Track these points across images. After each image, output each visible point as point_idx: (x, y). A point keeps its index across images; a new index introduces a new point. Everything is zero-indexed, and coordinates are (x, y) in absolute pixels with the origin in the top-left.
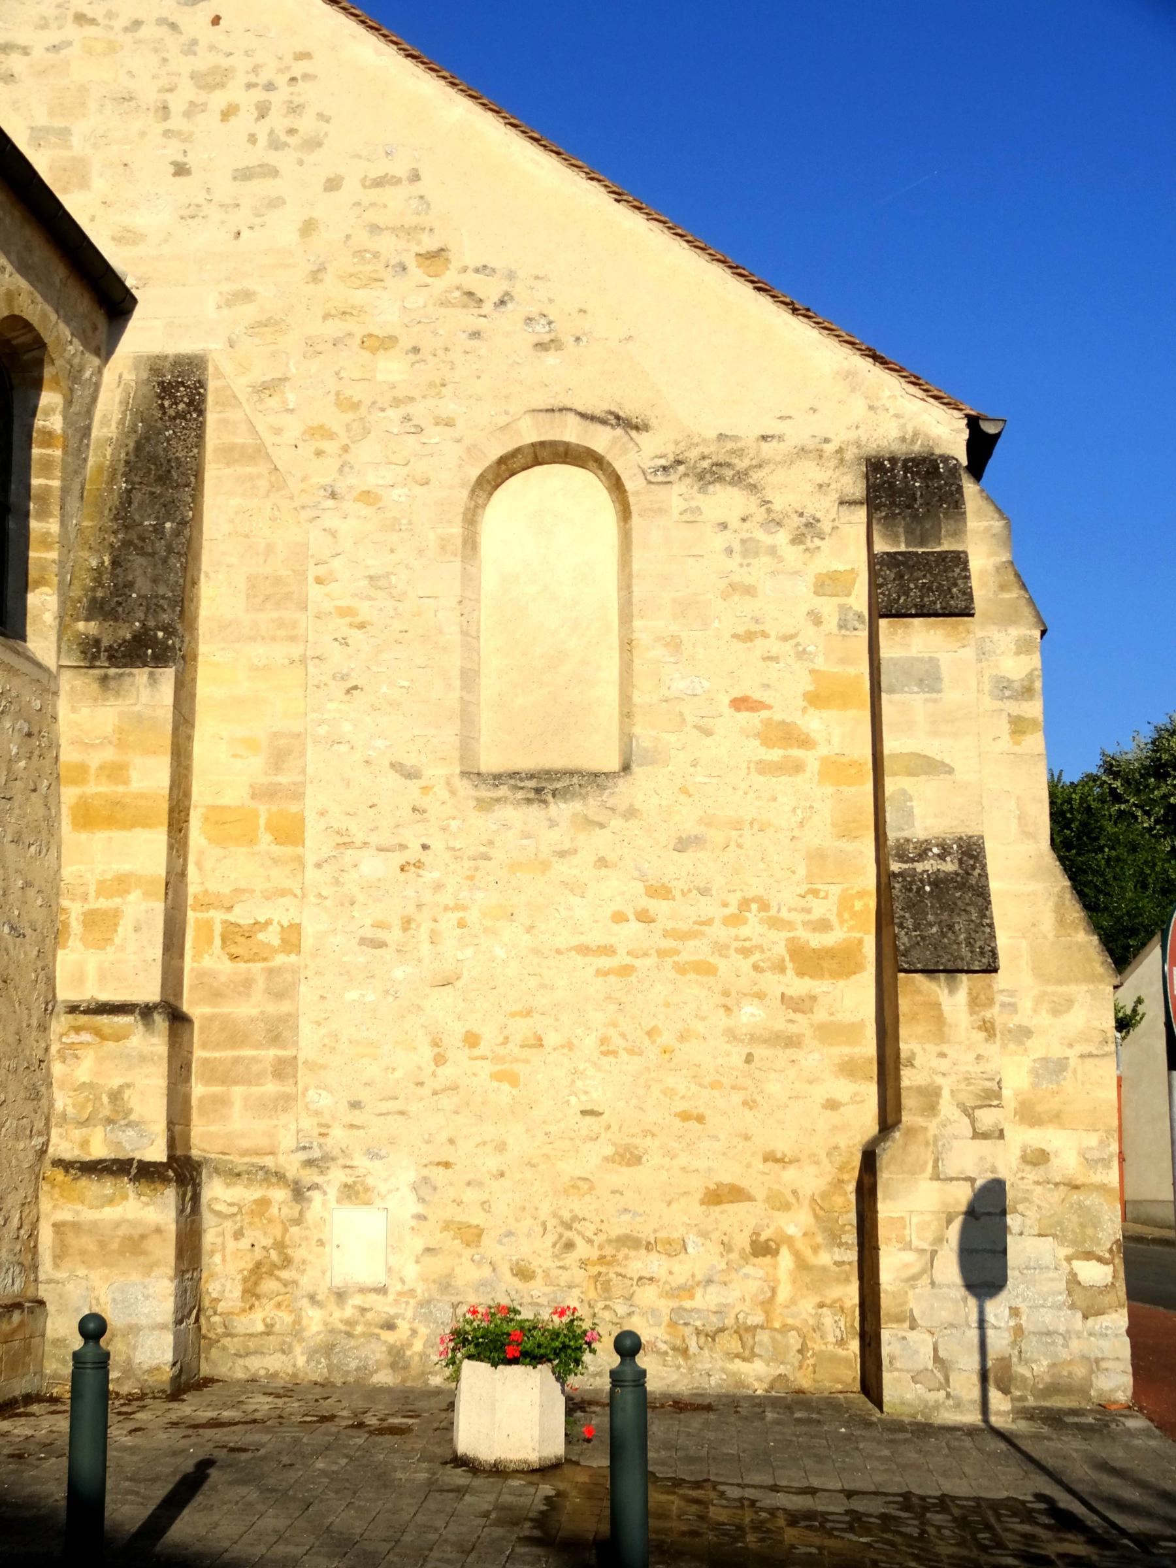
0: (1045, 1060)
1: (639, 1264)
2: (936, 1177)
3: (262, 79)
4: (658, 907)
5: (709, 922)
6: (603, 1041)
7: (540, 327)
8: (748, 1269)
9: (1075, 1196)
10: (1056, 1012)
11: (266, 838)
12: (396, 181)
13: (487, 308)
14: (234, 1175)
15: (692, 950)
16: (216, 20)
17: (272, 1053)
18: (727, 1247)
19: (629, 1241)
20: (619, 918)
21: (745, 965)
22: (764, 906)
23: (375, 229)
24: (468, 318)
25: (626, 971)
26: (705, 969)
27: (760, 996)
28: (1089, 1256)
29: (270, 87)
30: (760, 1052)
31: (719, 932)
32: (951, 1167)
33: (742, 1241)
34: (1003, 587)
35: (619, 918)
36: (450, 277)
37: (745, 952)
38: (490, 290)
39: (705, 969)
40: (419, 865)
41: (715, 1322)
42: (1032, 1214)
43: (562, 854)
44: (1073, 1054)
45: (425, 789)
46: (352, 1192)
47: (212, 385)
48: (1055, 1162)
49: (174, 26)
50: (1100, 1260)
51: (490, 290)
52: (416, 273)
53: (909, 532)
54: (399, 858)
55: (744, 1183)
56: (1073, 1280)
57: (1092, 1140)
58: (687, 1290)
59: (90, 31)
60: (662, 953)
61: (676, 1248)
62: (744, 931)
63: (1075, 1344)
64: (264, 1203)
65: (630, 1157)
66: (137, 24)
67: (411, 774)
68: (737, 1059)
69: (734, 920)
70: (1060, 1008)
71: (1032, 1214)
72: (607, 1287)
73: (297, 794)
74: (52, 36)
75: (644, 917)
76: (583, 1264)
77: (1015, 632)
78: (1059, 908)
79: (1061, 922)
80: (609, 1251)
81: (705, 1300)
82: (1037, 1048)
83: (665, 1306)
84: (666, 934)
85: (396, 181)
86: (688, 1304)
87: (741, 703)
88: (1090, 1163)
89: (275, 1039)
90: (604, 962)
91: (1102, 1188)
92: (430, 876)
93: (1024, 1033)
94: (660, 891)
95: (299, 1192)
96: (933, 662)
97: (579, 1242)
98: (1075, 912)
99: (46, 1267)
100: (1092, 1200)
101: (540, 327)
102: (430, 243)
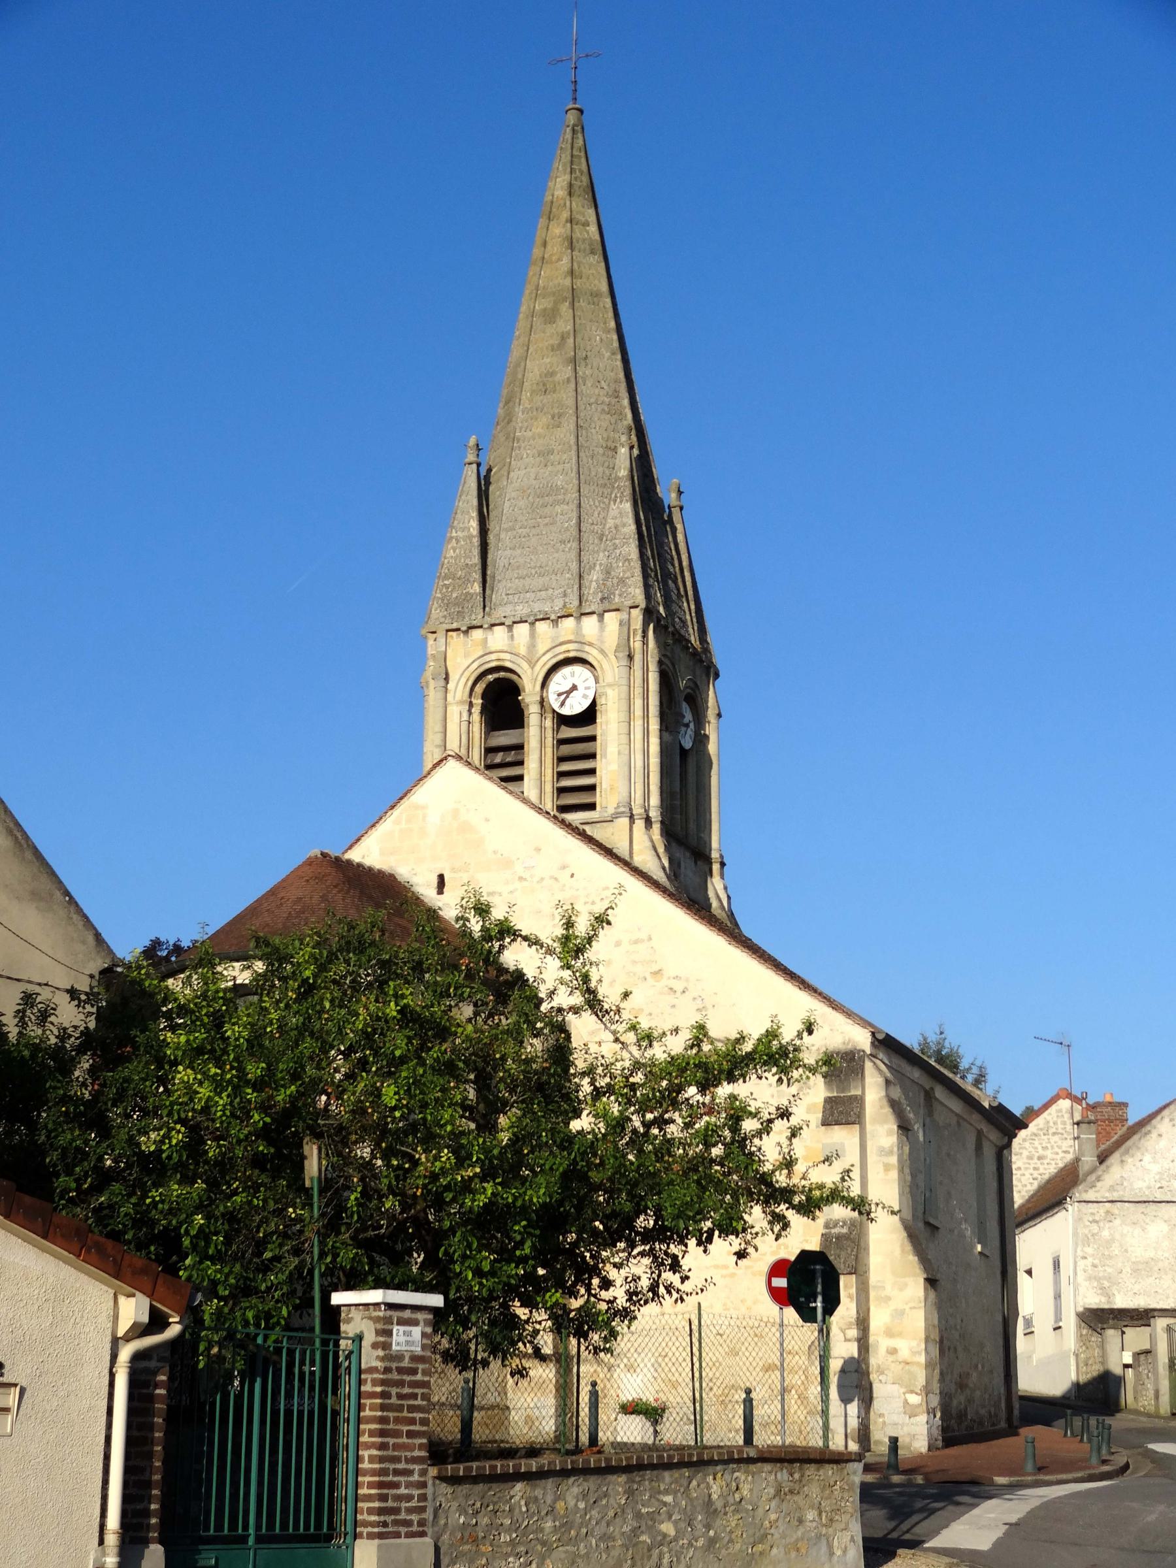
0: (896, 1310)
3: (590, 900)
7: (699, 1001)
9: (907, 1367)
10: (901, 1290)
12: (643, 941)
13: (678, 994)
16: (572, 876)
23: (634, 962)
24: (671, 999)
28: (912, 1392)
29: (593, 903)
34: (881, 1107)
36: (664, 982)
38: (679, 986)
42: (890, 1375)
44: (907, 1307)
46: (630, 1368)
48: (900, 1353)
49: (556, 879)
51: (679, 986)
52: (650, 980)
53: (838, 1087)
57: (914, 1343)
59: (525, 884)
63: (905, 1429)
65: (734, 1353)
66: (542, 879)
70: (902, 1288)
71: (890, 1375)
74: (511, 888)
77: (886, 1127)
78: (902, 1245)
79: (903, 1251)
82: (893, 1305)
85: (643, 941)
88: (914, 1353)
90: (724, 1272)
91: (918, 1364)
93: (888, 1298)
96: (842, 1144)
98: (909, 1247)
99: (510, 1394)
100: (914, 1369)
101: (699, 1001)
102: (655, 968)
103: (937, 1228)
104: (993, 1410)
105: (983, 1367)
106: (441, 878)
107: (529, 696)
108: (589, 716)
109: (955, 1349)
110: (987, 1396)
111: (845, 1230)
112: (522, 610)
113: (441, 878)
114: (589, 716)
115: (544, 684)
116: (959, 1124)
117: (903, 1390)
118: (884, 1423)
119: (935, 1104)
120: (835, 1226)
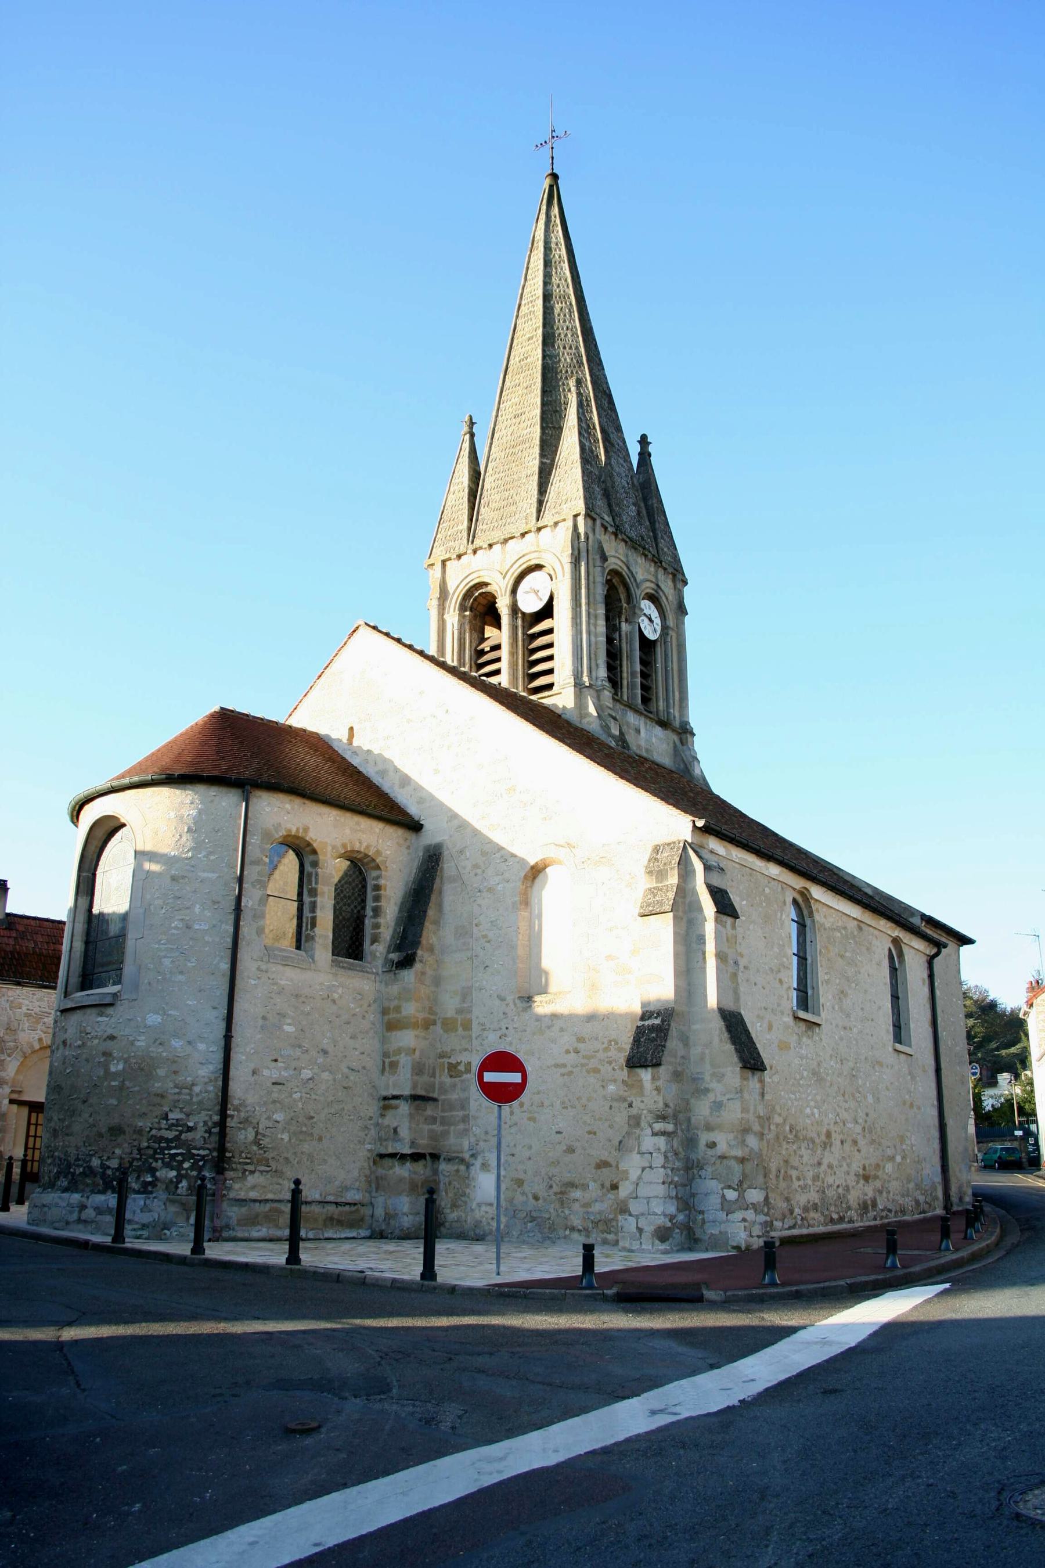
1: (577, 1194)
2: (639, 1153)
4: (581, 1046)
5: (597, 1051)
6: (563, 1103)
8: (609, 1196)
11: (460, 1029)
14: (449, 1160)
15: (593, 1063)
17: (461, 1113)
18: (603, 1186)
19: (572, 1185)
20: (568, 1052)
21: (610, 1068)
22: (616, 1043)
25: (570, 1073)
26: (596, 1071)
27: (615, 1081)
28: (730, 1187)
30: (615, 1104)
31: (601, 1055)
32: (644, 1149)
33: (608, 1184)
35: (568, 1052)
37: (610, 1063)
39: (596, 1071)
40: (505, 1035)
41: (598, 1217)
43: (549, 1028)
45: (507, 1005)
47: (446, 853)
50: (734, 1189)
54: (499, 1033)
55: (609, 1160)
56: (723, 1196)
58: (587, 1205)
60: (583, 1065)
61: (585, 1187)
62: (610, 1054)
64: (458, 1171)
65: (571, 1150)
67: (502, 999)
68: (607, 1108)
69: (606, 1050)
72: (562, 1204)
73: (469, 1011)
75: (577, 1052)
76: (556, 1194)
80: (563, 1189)
81: (597, 1207)
83: (582, 1210)
84: (584, 1057)
86: (590, 1210)
87: (609, 958)
89: (463, 1108)
90: (563, 1070)
92: (509, 1039)
94: (581, 1040)
95: (468, 1166)
97: (554, 1186)
103: (819, 1025)
104: (921, 1198)
105: (904, 1158)
106: (351, 729)
107: (503, 605)
108: (547, 611)
109: (855, 1142)
110: (911, 1186)
111: (657, 1021)
112: (498, 535)
113: (351, 729)
114: (547, 611)
115: (514, 591)
116: (860, 929)
117: (721, 1186)
118: (703, 1219)
119: (812, 902)
120: (649, 1018)
